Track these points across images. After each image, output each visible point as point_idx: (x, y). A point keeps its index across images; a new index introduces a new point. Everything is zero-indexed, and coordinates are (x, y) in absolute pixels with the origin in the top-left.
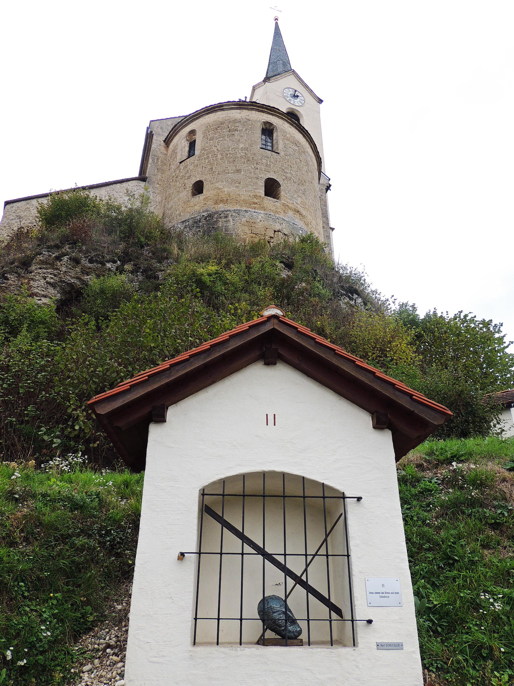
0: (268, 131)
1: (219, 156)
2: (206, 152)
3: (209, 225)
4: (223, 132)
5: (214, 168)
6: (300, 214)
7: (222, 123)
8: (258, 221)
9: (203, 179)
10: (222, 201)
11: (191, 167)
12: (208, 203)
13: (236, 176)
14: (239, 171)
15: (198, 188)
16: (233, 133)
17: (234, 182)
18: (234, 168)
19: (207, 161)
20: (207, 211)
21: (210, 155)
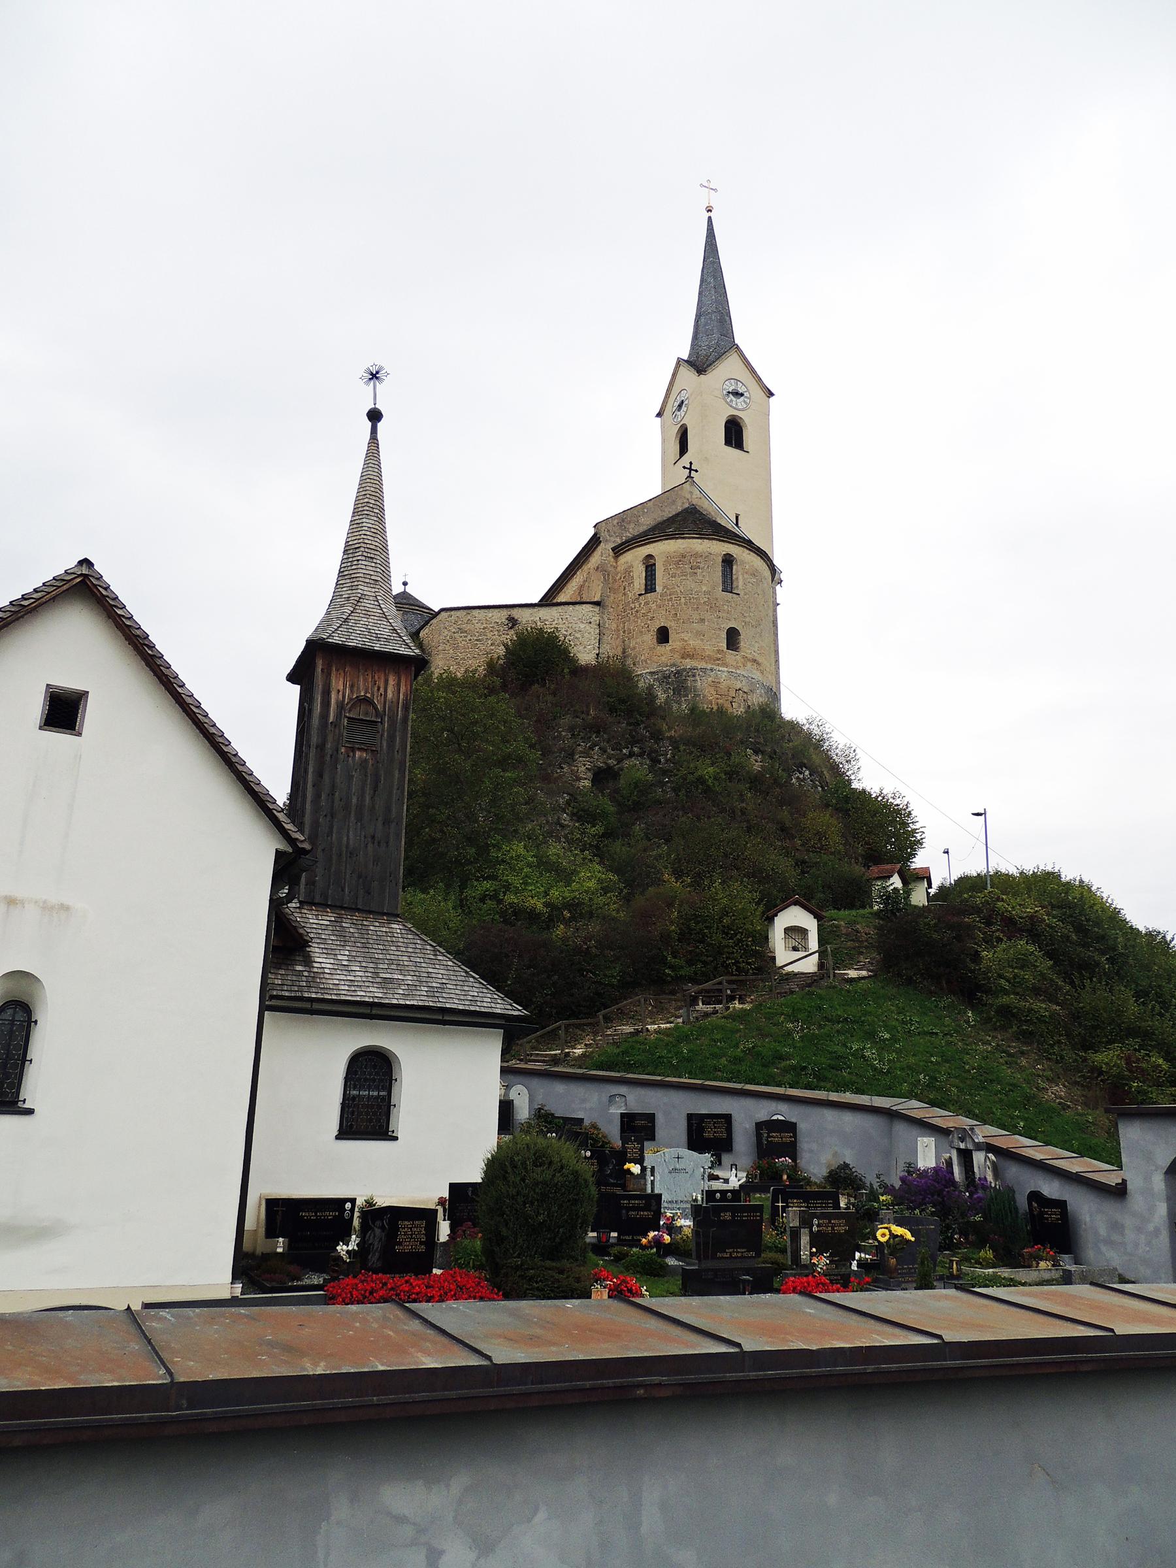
0: (728, 561)
3: (678, 681)
7: (684, 556)
10: (688, 656)
11: (654, 606)
14: (702, 620)
17: (699, 634)
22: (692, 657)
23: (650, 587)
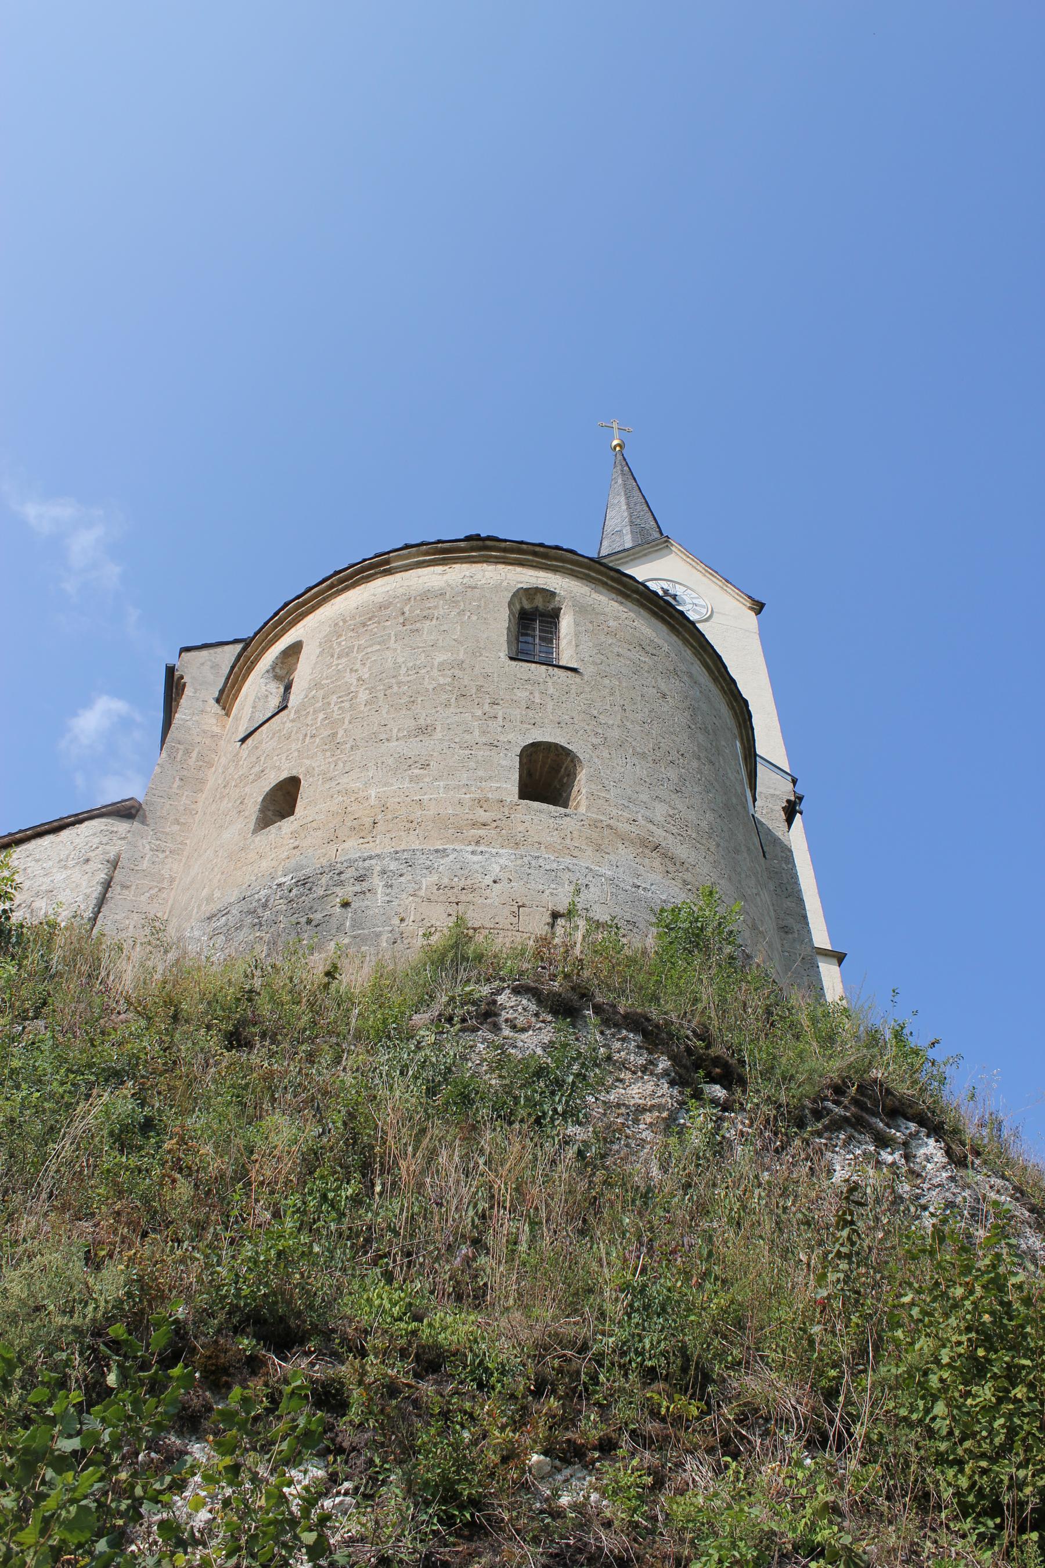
2: (321, 692)
4: (385, 628)
5: (341, 733)
6: (665, 855)
7: (381, 607)
8: (488, 880)
9: (298, 772)
12: (305, 843)
13: (414, 748)
14: (424, 730)
15: (283, 799)
19: (321, 716)
21: (334, 698)
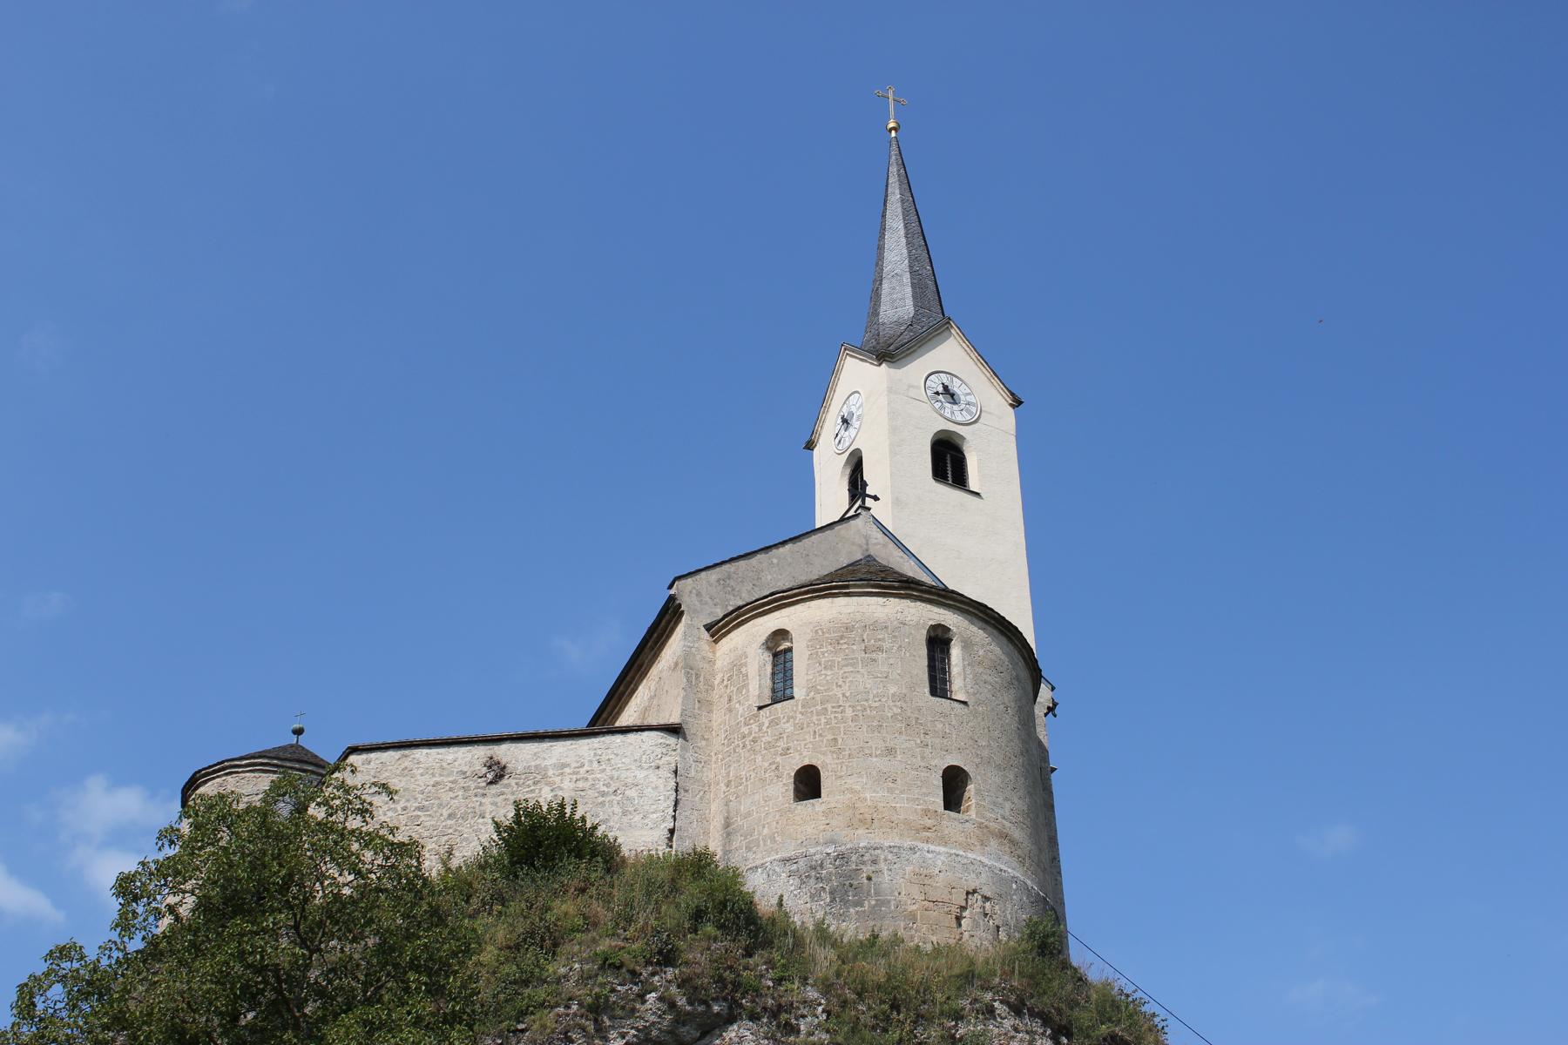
0: (938, 642)
1: (849, 713)
11: (789, 727)
16: (874, 655)
18: (881, 745)
20: (833, 842)
21: (829, 706)
22: (868, 823)
23: (781, 690)
